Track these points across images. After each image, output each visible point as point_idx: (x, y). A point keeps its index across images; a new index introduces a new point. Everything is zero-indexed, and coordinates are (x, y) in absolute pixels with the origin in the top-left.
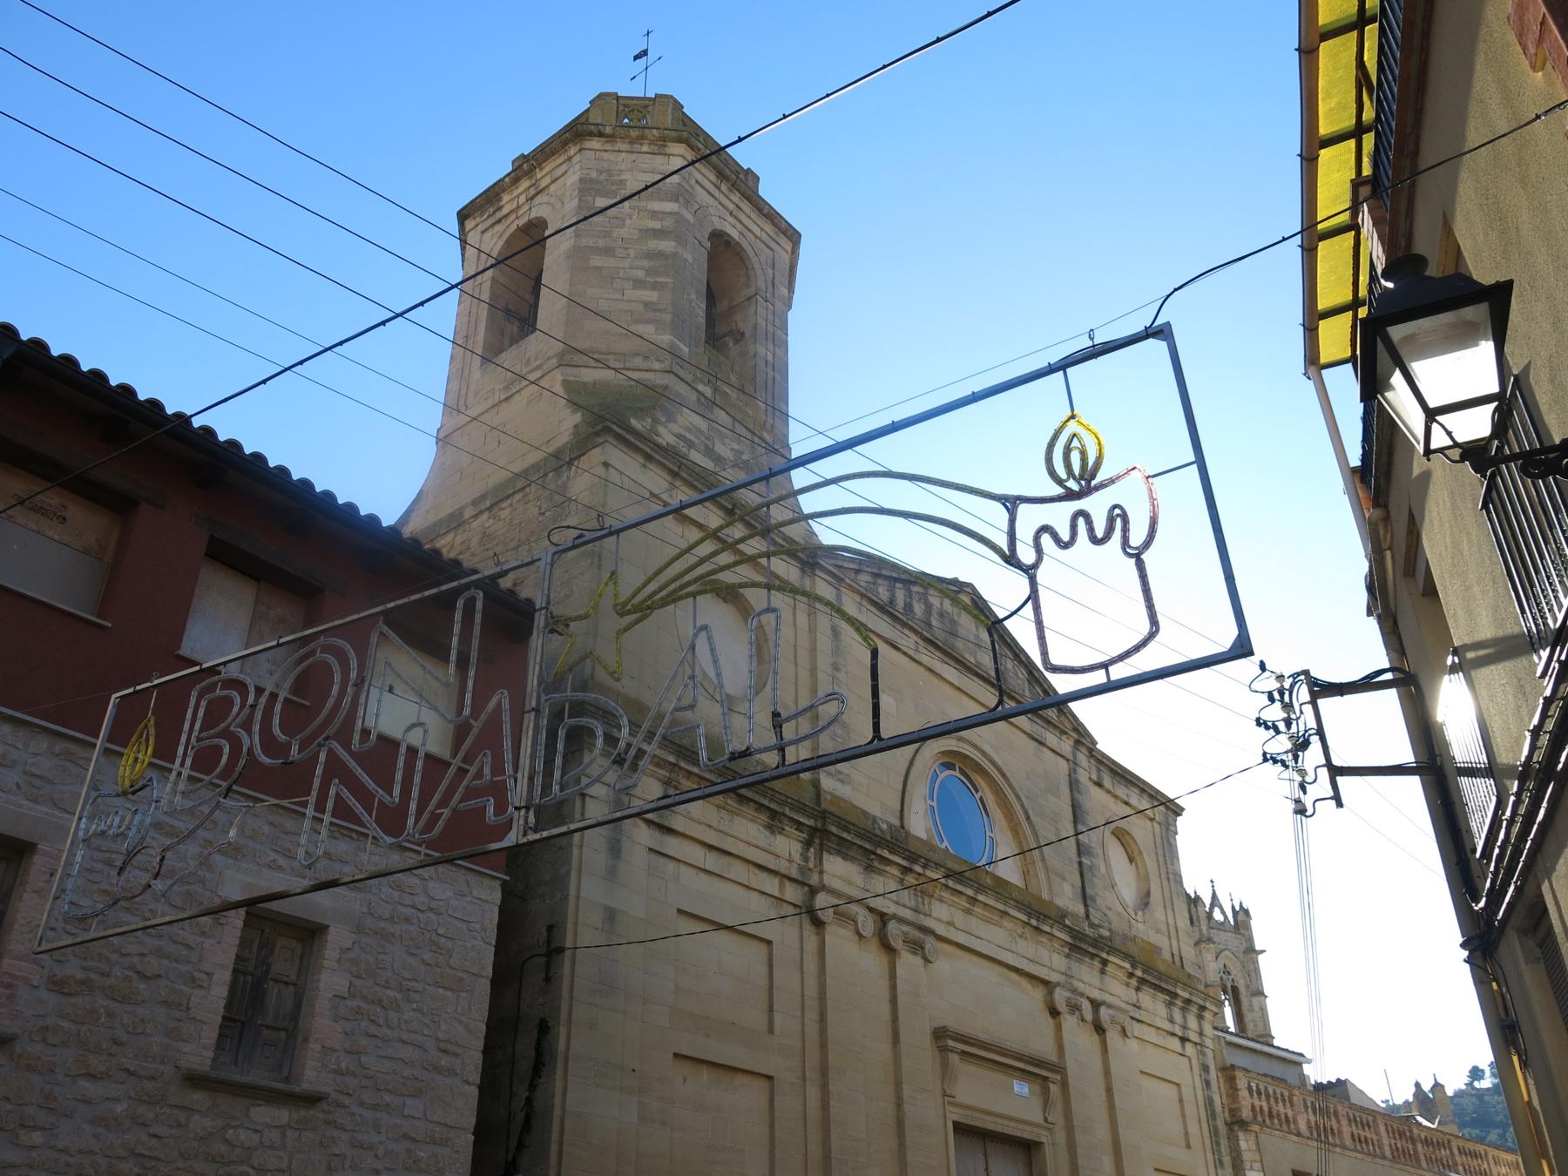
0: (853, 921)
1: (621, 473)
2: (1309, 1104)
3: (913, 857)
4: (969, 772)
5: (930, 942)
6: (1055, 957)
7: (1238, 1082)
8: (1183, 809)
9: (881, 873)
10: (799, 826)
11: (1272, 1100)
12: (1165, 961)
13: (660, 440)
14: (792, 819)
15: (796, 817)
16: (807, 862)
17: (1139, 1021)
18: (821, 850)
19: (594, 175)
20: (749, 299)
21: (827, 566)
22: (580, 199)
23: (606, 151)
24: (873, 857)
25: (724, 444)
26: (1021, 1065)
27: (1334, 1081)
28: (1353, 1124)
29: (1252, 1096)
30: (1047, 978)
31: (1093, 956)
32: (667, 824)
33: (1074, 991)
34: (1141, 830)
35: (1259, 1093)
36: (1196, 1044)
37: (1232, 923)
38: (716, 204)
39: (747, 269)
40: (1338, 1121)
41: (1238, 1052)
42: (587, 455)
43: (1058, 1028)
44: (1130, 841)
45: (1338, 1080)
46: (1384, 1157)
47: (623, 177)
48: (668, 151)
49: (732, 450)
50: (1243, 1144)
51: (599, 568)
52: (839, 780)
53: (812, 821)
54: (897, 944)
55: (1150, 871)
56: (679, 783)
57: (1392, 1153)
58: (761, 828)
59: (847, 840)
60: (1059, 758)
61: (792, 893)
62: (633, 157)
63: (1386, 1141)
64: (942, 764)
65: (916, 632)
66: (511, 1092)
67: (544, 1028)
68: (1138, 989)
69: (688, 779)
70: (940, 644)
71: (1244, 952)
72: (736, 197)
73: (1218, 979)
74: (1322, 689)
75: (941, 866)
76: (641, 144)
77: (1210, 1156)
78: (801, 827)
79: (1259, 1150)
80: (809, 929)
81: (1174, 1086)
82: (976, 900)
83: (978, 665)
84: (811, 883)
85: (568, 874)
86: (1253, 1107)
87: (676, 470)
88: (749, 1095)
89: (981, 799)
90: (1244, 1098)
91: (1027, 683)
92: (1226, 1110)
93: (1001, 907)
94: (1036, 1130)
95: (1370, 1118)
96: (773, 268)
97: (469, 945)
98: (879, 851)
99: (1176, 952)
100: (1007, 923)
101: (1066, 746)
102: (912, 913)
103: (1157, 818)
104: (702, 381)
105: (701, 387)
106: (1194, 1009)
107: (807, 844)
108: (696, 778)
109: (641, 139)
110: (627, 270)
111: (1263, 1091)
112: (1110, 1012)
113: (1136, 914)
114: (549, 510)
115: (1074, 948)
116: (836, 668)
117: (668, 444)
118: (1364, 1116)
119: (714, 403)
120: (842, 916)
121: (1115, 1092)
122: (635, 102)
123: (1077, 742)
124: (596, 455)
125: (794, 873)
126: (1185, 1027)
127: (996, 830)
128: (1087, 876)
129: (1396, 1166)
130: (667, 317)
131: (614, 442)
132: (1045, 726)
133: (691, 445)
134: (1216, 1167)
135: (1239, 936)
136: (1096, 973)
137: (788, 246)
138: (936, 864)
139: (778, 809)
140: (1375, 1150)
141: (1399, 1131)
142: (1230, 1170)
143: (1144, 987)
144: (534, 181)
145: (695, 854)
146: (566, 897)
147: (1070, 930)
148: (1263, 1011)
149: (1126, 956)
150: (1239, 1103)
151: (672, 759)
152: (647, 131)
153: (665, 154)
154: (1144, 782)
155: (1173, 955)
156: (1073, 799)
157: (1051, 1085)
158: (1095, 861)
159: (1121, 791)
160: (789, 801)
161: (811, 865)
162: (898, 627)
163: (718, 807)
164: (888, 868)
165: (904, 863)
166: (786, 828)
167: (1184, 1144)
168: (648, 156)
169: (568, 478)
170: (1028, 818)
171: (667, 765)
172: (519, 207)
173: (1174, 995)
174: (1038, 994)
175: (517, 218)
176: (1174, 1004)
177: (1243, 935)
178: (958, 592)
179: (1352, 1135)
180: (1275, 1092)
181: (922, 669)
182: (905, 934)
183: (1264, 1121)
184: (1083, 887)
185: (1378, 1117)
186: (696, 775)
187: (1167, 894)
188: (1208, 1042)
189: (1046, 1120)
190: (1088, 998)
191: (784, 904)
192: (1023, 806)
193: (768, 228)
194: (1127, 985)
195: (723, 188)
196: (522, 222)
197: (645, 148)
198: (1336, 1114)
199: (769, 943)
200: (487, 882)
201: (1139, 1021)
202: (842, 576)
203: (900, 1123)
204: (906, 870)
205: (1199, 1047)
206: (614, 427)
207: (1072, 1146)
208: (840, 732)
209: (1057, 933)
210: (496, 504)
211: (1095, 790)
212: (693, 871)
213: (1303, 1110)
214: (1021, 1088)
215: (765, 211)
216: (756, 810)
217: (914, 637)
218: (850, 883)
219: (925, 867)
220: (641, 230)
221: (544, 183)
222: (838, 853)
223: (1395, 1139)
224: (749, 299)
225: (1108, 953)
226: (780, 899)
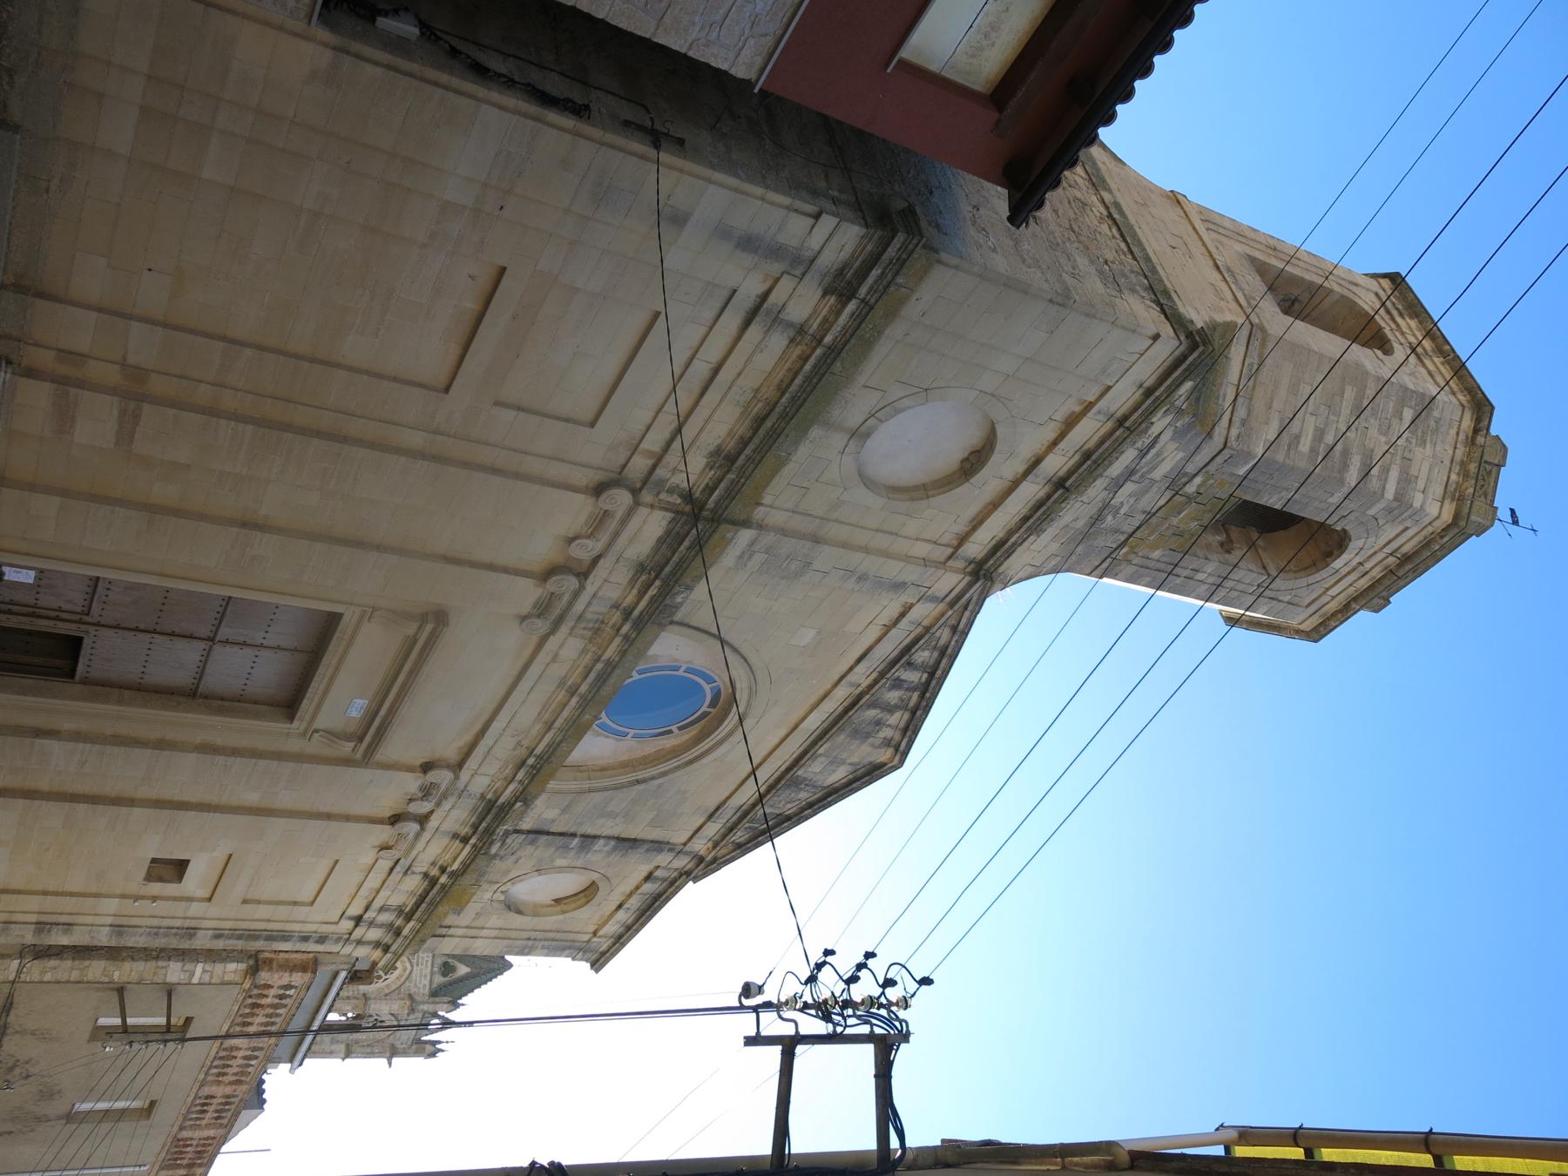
0: (592, 533)
1: (1142, 355)
2: (256, 1053)
3: (640, 625)
4: (702, 723)
5: (542, 626)
6: (486, 781)
7: (300, 974)
8: (597, 971)
9: (633, 581)
10: (710, 489)
11: (271, 1011)
12: (446, 915)
13: (1160, 413)
14: (720, 481)
15: (722, 485)
16: (668, 492)
17: (392, 869)
18: (677, 512)
19: (1436, 414)
20: (1264, 568)
21: (972, 591)
22: (1413, 392)
23: (1458, 434)
24: (653, 574)
25: (1130, 496)
26: (383, 712)
27: (264, 1096)
28: (223, 1101)
29: (281, 987)
30: (466, 766)
31: (475, 827)
32: (757, 319)
33: (445, 796)
34: (584, 919)
35: (281, 997)
36: (350, 934)
37: (424, 1038)
38: (1376, 548)
39: (1296, 572)
40: (231, 1083)
41: (326, 980)
42: (1167, 322)
43: (409, 769)
44: (579, 903)
45: (264, 1101)
46: (181, 1128)
47: (1428, 445)
48: (1447, 502)
49: (1122, 503)
50: (232, 966)
51: (1050, 301)
52: (743, 552)
53: (712, 506)
54: (552, 585)
55: (542, 918)
56: (797, 345)
57: (182, 1140)
58: (719, 441)
59: (680, 544)
60: (689, 834)
61: (640, 464)
62: (1447, 462)
63: (198, 1134)
64: (719, 691)
65: (871, 687)
66: (509, 56)
67: (579, 111)
68: (426, 875)
69: (799, 357)
70: (850, 714)
71: (393, 1045)
72: (1377, 573)
73: (371, 1012)
74: (886, 1048)
76: (1458, 474)
77: (229, 924)
78: (708, 491)
79: (222, 984)
80: (597, 477)
81: (311, 899)
82: (573, 695)
83: (814, 757)
84: (644, 492)
85: (736, 175)
86: (270, 987)
87: (1127, 424)
88: (432, 358)
89: (670, 732)
90: (280, 978)
91: (778, 812)
92: (272, 956)
93: (557, 724)
94: (307, 717)
95: (225, 1121)
96: (1289, 603)
97: (697, 19)
98: (658, 583)
99: (451, 931)
100: (538, 727)
101: (700, 846)
102: (579, 613)
103: (595, 939)
104: (1204, 482)
105: (1198, 480)
106: (387, 939)
107: (688, 496)
109: (1465, 474)
110: (1335, 426)
111: (284, 1001)
112: (411, 836)
113: (502, 892)
114: (1110, 270)
115: (491, 804)
116: (862, 578)
117: (1152, 423)
118: (229, 1114)
119: (1177, 493)
120: (600, 520)
121: (325, 823)
122: (1492, 483)
123: (701, 859)
124: (1167, 330)
125: (660, 472)
126: (371, 924)
127: (633, 743)
128: (560, 841)
129: (170, 1140)
130: (1280, 457)
131: (1177, 353)
132: (728, 825)
133: (1143, 453)
134: (215, 929)
135: (409, 1043)
136: (456, 828)
137: (1306, 626)
138: (625, 651)
139: (736, 465)
140: (191, 1119)
141: (204, 1151)
142: (208, 946)
143: (426, 883)
144: (1430, 354)
145: (712, 352)
146: (713, 167)
147: (510, 805)
148: (329, 1054)
149: (465, 867)
150: (277, 971)
151: (828, 339)
152: (1473, 482)
153: (1444, 498)
154: (638, 931)
155: (449, 927)
156: (643, 841)
157: (352, 745)
158: (572, 853)
159: (635, 903)
160: (743, 480)
161: (663, 496)
162: (882, 667)
163: (757, 391)
164: (635, 591)
165: (636, 612)
166: (713, 472)
167: (249, 897)
168: (1445, 478)
169: (1143, 297)
170: (638, 782)
172: (1403, 333)
173: (409, 918)
174: (451, 753)
175: (1392, 330)
176: (398, 916)
177: (410, 1047)
178: (897, 750)
179: (213, 1097)
180: (278, 1015)
181: (829, 687)
182: (560, 596)
183: (250, 997)
184: (548, 833)
185: (226, 1130)
186: (802, 367)
187: (514, 934)
188: (347, 949)
189: (316, 731)
190: (432, 812)
191: (629, 453)
192: (652, 778)
193: (1333, 606)
194: (433, 864)
195: (1391, 560)
196: (1387, 331)
197: (1454, 477)
198: (238, 1082)
199: (592, 424)
200: (759, 61)
201: (392, 869)
202: (956, 607)
203: (358, 544)
204: (627, 614)
205: (346, 936)
206: (1195, 355)
207: (279, 756)
208: (793, 567)
209: (512, 787)
210: (1116, 223)
211: (644, 870)
212: (695, 343)
213: (252, 1045)
214: (358, 708)
215: (1354, 605)
216: (742, 438)
217: (866, 683)
218: (631, 541)
219: (626, 637)
220: (1372, 451)
221: (1427, 362)
222: (668, 533)
223: (197, 1146)
224: (1264, 568)
225: (474, 846)
226: (636, 449)
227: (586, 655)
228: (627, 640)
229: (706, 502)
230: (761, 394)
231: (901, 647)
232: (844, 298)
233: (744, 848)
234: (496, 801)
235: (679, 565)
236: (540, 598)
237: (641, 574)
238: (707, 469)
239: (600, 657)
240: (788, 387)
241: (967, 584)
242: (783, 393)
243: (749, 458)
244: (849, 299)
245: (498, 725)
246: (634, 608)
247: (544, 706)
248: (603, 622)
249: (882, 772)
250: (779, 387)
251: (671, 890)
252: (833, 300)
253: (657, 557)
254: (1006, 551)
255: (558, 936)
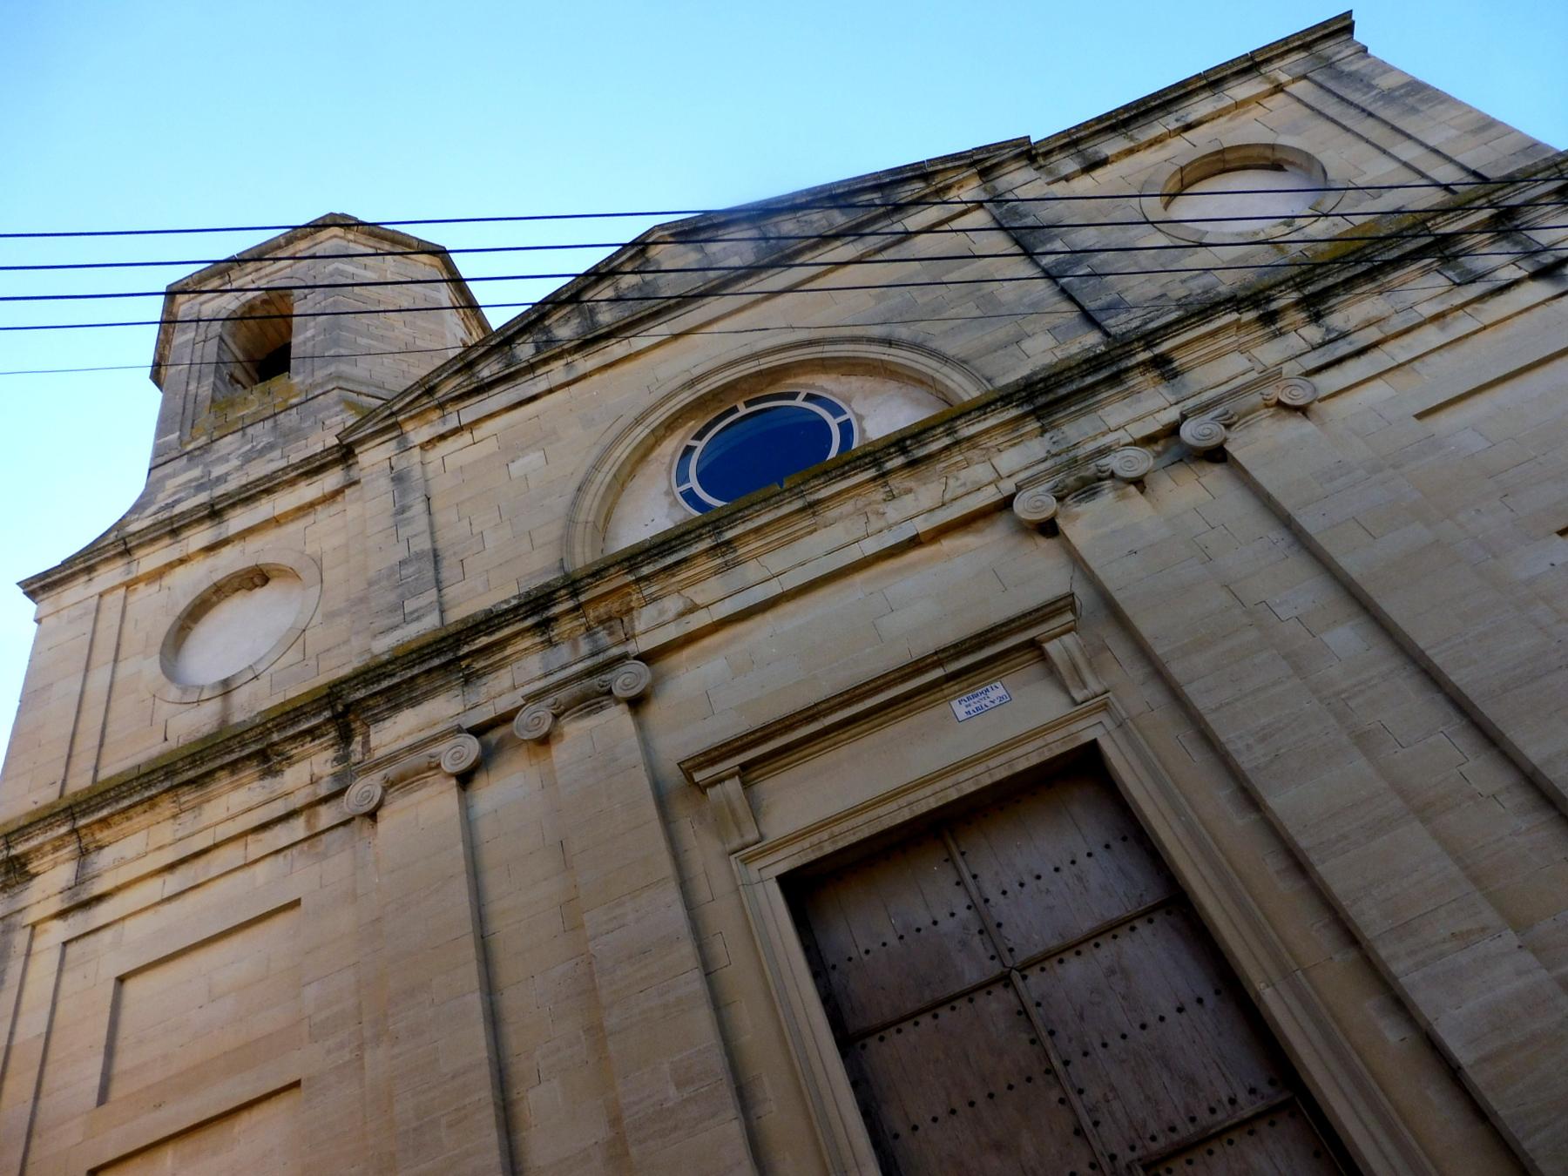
10: (312, 733)
14: (294, 738)
24: (464, 664)
26: (938, 673)
56: (98, 841)
59: (398, 685)
69: (109, 826)
75: (606, 568)
82: (728, 543)
93: (798, 504)
98: (461, 653)
108: (116, 818)
115: (1039, 413)
164: (509, 651)
171: (67, 839)
181: (596, 378)
216: (233, 773)
228: (575, 590)
229: (328, 720)
230: (174, 810)
231: (486, 395)
232: (23, 860)
233: (918, 173)
237: (478, 670)
238: (294, 759)
239: (638, 581)
240: (141, 802)
241: (364, 444)
242: (151, 798)
243: (243, 746)
244: (17, 857)
245: (889, 540)
246: (528, 630)
247: (794, 540)
249: (681, 226)
250: (152, 807)
251: (1082, 134)
252: (32, 868)
254: (309, 463)
255: (1333, 109)
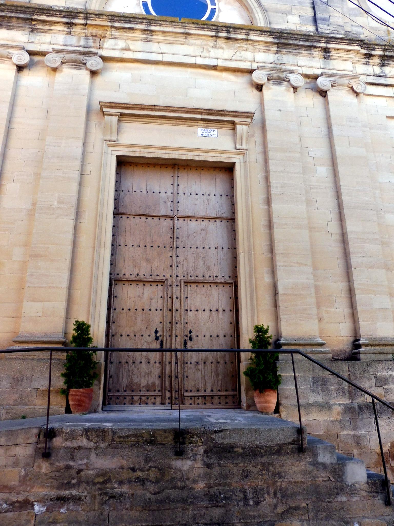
24: (34, 23)
26: (199, 116)
31: (310, 48)
68: (382, 65)
82: (151, 31)
93: (182, 30)
100: (192, 41)
115: (279, 45)
138: (96, 15)
164: (52, 28)
174: (241, 80)
225: (327, 42)
227: (115, 35)
228: (87, 17)
234: (274, 43)
235: (17, 11)
236: (71, 68)
237: (38, 29)
245: (200, 61)
248: (86, 36)
253: (20, 25)
